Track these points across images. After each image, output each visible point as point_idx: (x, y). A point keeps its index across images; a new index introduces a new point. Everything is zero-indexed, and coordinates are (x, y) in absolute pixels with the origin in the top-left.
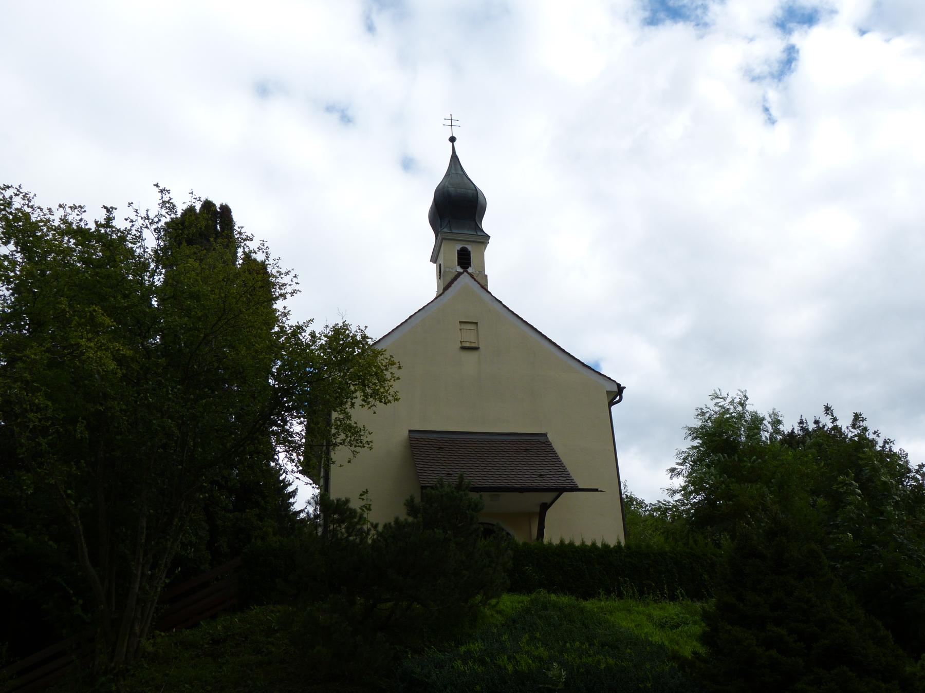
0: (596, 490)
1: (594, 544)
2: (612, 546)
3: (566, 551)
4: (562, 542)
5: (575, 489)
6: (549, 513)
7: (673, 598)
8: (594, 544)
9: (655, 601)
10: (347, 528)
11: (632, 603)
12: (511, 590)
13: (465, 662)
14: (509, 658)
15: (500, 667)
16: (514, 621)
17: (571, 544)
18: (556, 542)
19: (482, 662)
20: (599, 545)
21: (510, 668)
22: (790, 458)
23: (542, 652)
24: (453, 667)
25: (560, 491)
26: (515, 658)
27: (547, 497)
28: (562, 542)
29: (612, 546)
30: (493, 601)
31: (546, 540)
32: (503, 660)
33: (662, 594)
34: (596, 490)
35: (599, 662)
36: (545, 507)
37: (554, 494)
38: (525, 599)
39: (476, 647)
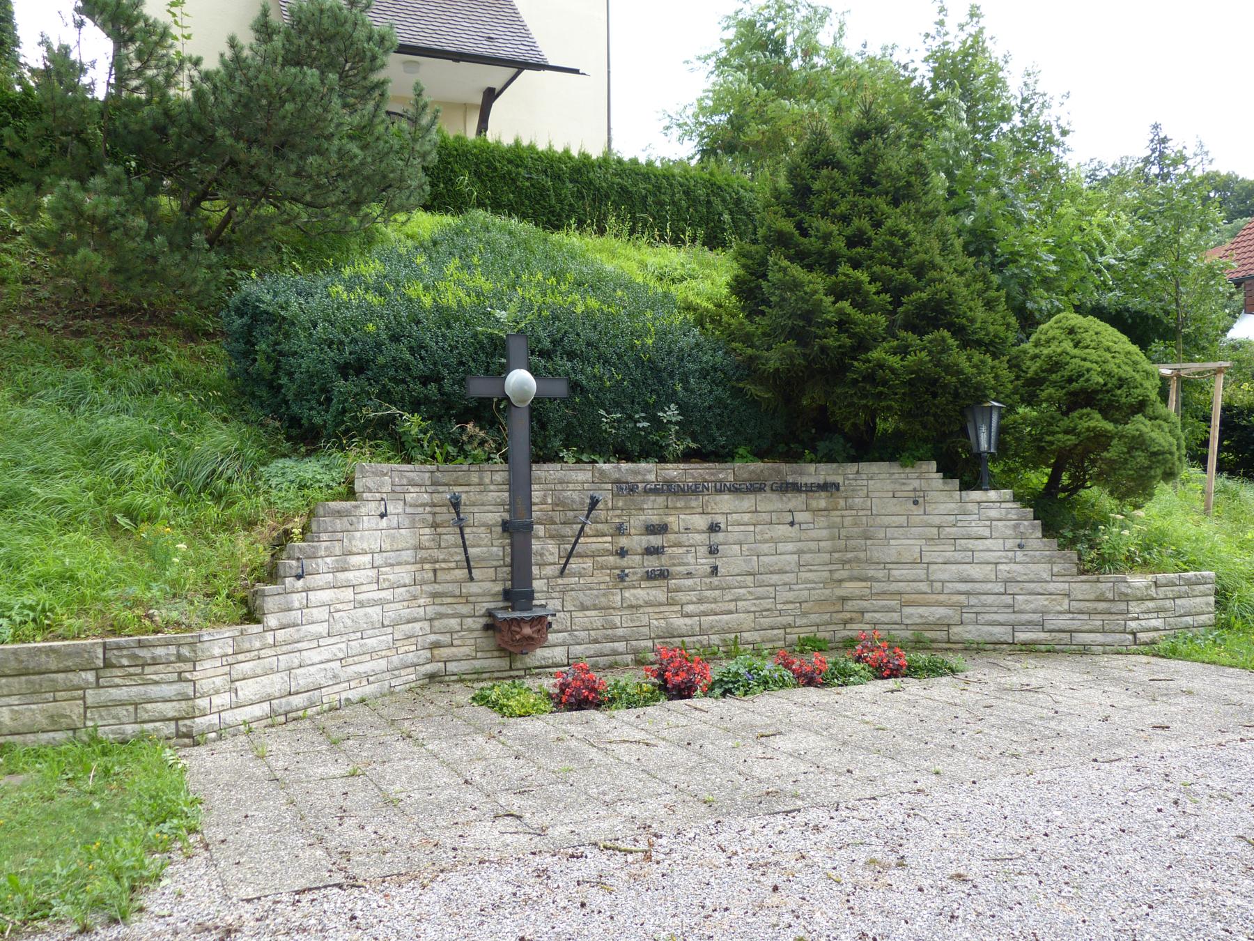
0: (576, 71)
1: (566, 151)
2: (594, 157)
3: (519, 157)
4: (517, 143)
5: (540, 66)
6: (497, 106)
7: (677, 241)
8: (566, 151)
9: (650, 244)
10: (139, 54)
11: (616, 243)
12: (426, 208)
13: (350, 289)
14: (426, 288)
15: (410, 300)
16: (435, 243)
17: (531, 148)
18: (508, 141)
19: (381, 291)
20: (575, 153)
21: (427, 301)
22: (651, 402)
23: (482, 283)
24: (329, 296)
25: (521, 66)
26: (434, 286)
27: (495, 76)
28: (517, 143)
29: (594, 157)
30: (401, 217)
31: (491, 136)
32: (415, 290)
33: (661, 237)
34: (576, 71)
35: (573, 304)
36: (491, 95)
37: (511, 71)
38: (448, 219)
39: (371, 268)
